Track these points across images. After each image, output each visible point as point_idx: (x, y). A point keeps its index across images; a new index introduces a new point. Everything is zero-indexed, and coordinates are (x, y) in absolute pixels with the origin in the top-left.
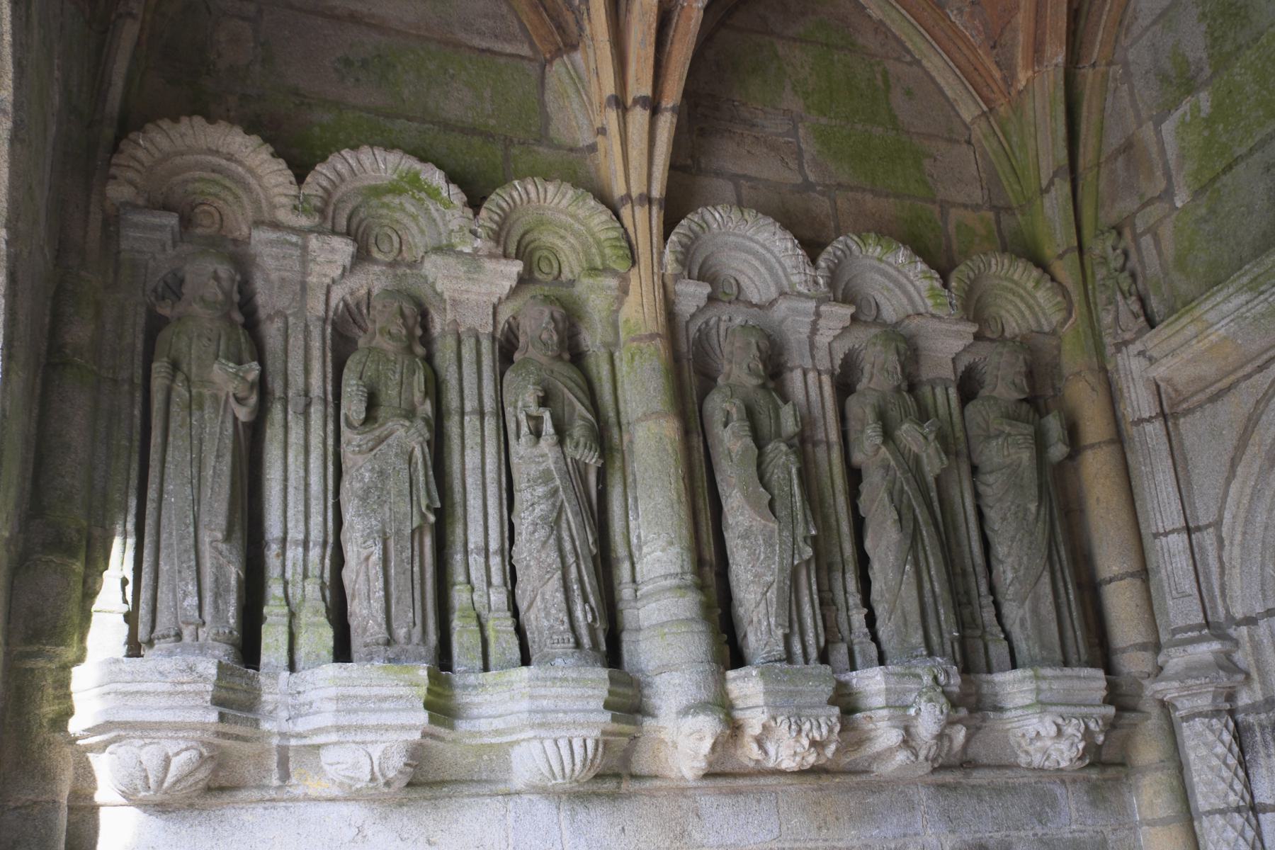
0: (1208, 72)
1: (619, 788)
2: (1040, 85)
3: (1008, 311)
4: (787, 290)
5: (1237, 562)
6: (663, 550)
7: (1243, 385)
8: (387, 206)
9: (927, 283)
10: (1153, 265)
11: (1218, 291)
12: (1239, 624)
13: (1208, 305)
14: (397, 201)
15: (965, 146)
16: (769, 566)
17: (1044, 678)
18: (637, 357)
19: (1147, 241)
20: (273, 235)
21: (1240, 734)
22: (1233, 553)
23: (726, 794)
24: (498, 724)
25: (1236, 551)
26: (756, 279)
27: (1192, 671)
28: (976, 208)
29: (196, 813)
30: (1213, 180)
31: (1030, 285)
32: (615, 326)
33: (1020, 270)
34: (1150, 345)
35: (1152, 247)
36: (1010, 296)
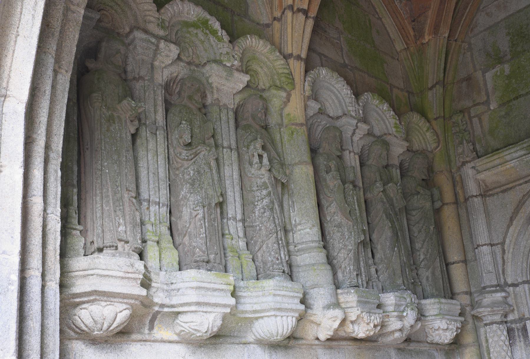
0: (509, 57)
1: (289, 343)
2: (434, 43)
3: (415, 139)
4: (346, 113)
5: (510, 260)
6: (310, 229)
7: (518, 188)
8: (189, 32)
9: (394, 121)
10: (478, 131)
11: (512, 148)
12: (510, 286)
13: (507, 152)
14: (195, 32)
15: (397, 61)
16: (350, 242)
17: (442, 303)
18: (295, 133)
19: (475, 120)
20: (144, 36)
21: (510, 331)
22: (508, 256)
23: (327, 349)
24: (257, 307)
25: (510, 256)
26: (332, 105)
27: (494, 304)
28: (402, 90)
29: (109, 345)
30: (509, 102)
31: (425, 129)
32: (281, 115)
33: (423, 122)
34: (478, 164)
35: (478, 123)
36: (417, 133)
